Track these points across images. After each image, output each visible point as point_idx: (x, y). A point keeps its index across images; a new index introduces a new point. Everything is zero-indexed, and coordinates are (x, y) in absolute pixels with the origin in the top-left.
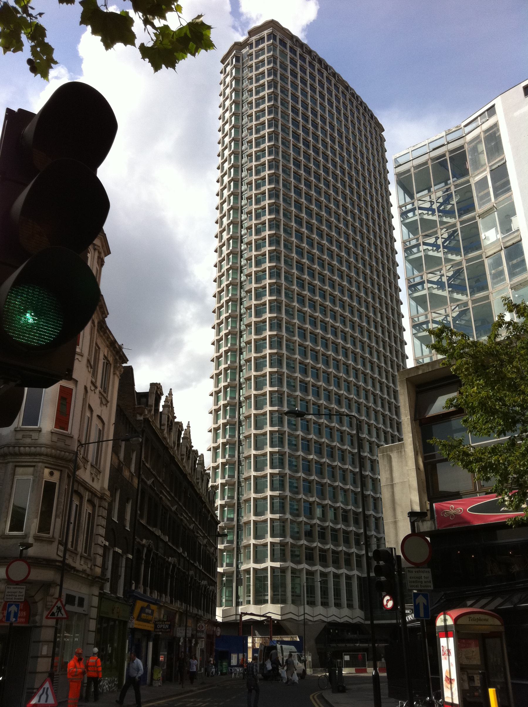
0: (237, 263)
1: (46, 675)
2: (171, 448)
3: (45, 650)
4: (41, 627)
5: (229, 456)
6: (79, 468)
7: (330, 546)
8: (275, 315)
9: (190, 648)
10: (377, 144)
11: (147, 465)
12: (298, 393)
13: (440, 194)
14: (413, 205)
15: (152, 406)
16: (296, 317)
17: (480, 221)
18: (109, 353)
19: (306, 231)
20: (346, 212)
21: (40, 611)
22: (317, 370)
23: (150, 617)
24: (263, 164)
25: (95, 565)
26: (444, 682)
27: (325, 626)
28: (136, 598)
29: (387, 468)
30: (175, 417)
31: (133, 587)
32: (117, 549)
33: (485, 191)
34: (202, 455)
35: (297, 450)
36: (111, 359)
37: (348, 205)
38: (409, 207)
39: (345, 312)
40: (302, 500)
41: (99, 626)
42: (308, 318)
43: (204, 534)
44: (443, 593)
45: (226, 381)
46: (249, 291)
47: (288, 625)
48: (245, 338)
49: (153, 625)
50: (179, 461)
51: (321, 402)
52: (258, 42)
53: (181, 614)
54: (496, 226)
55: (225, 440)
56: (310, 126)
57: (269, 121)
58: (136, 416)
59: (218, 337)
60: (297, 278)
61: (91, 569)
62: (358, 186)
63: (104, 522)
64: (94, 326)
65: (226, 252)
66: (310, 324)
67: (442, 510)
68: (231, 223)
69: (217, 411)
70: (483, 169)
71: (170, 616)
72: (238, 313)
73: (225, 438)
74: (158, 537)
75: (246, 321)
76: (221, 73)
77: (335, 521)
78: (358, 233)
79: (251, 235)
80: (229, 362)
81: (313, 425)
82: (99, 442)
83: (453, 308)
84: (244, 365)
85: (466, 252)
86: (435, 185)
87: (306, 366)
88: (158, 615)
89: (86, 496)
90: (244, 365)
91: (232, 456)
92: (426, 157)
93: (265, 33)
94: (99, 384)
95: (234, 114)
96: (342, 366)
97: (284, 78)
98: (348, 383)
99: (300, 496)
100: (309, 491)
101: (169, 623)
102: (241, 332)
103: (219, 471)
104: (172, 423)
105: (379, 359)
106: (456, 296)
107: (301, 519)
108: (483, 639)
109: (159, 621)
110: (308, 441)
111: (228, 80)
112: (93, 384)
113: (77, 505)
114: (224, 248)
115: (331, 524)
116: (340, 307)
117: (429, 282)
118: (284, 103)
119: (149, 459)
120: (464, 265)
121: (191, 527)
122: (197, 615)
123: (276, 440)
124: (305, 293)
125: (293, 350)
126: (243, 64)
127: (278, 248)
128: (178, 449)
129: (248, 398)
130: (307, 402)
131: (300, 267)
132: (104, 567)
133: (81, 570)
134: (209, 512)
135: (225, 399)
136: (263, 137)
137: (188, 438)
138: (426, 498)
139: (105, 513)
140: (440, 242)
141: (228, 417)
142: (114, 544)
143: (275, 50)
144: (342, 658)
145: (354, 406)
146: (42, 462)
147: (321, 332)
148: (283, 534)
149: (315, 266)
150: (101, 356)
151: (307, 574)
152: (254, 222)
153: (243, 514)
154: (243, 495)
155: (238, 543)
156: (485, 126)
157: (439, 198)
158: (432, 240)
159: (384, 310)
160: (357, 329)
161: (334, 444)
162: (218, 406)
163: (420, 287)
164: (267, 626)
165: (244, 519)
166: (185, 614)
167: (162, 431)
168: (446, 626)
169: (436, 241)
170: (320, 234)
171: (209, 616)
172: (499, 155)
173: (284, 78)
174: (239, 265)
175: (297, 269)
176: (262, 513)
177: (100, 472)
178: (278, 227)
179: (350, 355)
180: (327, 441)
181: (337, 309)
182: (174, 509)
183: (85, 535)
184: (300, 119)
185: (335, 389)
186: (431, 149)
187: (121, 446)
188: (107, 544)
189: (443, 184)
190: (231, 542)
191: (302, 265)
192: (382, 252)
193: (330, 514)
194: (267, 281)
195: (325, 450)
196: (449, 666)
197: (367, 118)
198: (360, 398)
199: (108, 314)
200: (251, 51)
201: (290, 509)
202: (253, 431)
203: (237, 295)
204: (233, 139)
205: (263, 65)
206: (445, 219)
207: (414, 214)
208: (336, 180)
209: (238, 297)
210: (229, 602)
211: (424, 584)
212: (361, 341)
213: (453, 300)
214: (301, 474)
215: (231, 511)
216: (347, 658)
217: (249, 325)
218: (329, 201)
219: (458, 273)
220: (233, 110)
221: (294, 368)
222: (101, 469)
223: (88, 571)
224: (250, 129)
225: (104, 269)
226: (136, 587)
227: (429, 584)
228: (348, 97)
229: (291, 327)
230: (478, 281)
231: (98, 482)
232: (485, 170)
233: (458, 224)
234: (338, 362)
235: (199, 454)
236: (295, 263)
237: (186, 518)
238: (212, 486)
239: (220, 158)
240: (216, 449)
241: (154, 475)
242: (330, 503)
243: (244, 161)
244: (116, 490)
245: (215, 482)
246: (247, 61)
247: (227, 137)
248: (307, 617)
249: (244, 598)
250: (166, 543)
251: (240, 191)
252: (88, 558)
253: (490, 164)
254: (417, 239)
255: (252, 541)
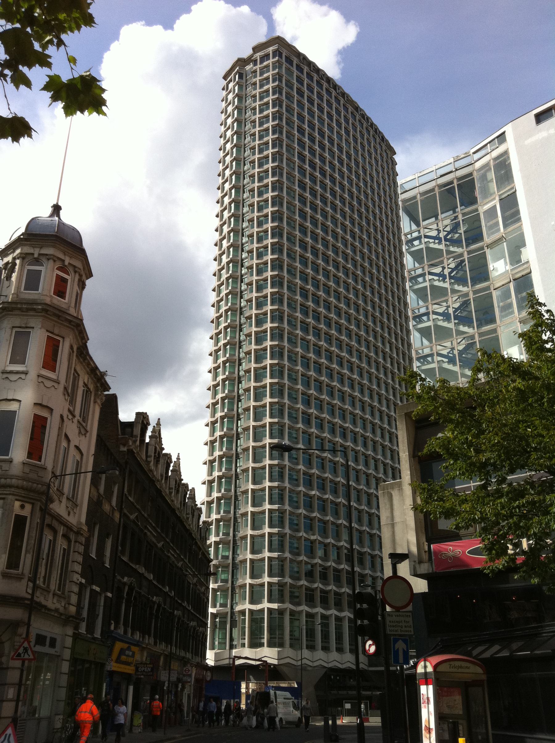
0: (237, 288)
1: (10, 720)
2: (158, 481)
3: (11, 693)
4: (7, 668)
5: (225, 490)
6: (52, 501)
7: (332, 587)
8: (276, 343)
9: (176, 692)
10: (388, 168)
11: (130, 498)
12: (300, 425)
13: (447, 222)
14: (419, 233)
15: (137, 436)
16: (299, 345)
17: (488, 252)
18: (90, 380)
19: (311, 257)
20: (354, 238)
21: (6, 651)
22: (321, 401)
23: (130, 660)
24: (266, 186)
25: (69, 604)
26: (423, 732)
27: (326, 673)
28: (115, 639)
29: (388, 506)
30: (163, 449)
31: (112, 627)
32: (94, 587)
33: (494, 221)
34: (193, 489)
35: (298, 485)
36: (91, 387)
37: (356, 230)
38: (415, 235)
39: (352, 341)
40: (303, 539)
41: (73, 669)
42: (312, 347)
43: (194, 572)
44: (439, 639)
45: (223, 411)
46: (250, 318)
47: (285, 669)
48: (244, 366)
49: (134, 668)
50: (166, 494)
51: (325, 435)
52: (263, 59)
53: (166, 656)
54: (505, 257)
55: (221, 474)
56: (317, 147)
57: (273, 141)
58: (119, 447)
59: (216, 365)
60: (301, 305)
61: (65, 608)
62: (368, 211)
63: (80, 559)
64: (73, 352)
65: (226, 276)
66: (314, 353)
67: (440, 551)
68: (232, 245)
69: (212, 442)
70: (492, 197)
71: (154, 659)
72: (237, 340)
73: (221, 471)
74: (142, 575)
75: (245, 348)
76: (223, 89)
77: (338, 561)
78: (367, 260)
79: (252, 259)
80: (226, 392)
81: (315, 459)
82: (77, 473)
83: (459, 340)
84: (243, 395)
85: (474, 283)
86: (442, 213)
87: (309, 396)
88: (139, 656)
89: (61, 530)
90: (243, 395)
91: (228, 490)
92: (433, 184)
93: (271, 49)
94: (77, 412)
95: (236, 132)
96: (348, 397)
97: (289, 97)
98: (354, 416)
99: (301, 534)
100: (310, 528)
101: (151, 666)
102: (240, 360)
103: (214, 505)
104: (159, 454)
105: (387, 391)
106: (462, 328)
107: (301, 558)
108: (466, 687)
109: (141, 664)
110: (310, 476)
111: (230, 97)
112: (71, 413)
113: (50, 540)
114: (224, 272)
115: (333, 564)
116: (346, 337)
117: (434, 313)
118: (289, 123)
119: (133, 492)
120: (471, 296)
121: (180, 564)
122: (184, 658)
123: (276, 474)
124: (309, 320)
125: (295, 380)
126: (246, 81)
127: (281, 274)
128: (166, 482)
129: (247, 429)
130: (309, 435)
131: (305, 294)
132: (79, 606)
133: (53, 608)
134: (200, 549)
135: (222, 430)
136: (267, 157)
137: (177, 471)
138: (424, 539)
139: (81, 549)
140: (446, 272)
141: (224, 449)
142: (91, 582)
143: (280, 67)
144: (342, 706)
145: (360, 440)
146: (13, 495)
147: (325, 362)
148: (281, 574)
149: (320, 293)
150: (81, 384)
151: (306, 617)
152: (255, 245)
153: (239, 552)
154: (239, 532)
155: (232, 582)
156: (495, 154)
157: (446, 226)
158: (438, 270)
159: (394, 340)
160: (364, 359)
161: (338, 479)
162: (214, 438)
163: (425, 318)
164: (263, 671)
165: (240, 557)
166: (169, 657)
167: (148, 463)
168: (426, 673)
169: (443, 271)
170: (326, 259)
171: (198, 659)
172: (509, 184)
173: (289, 97)
174: (239, 290)
175: (301, 296)
176: (260, 552)
177: (77, 506)
178: (281, 251)
179: (357, 387)
180: (330, 476)
181: (343, 338)
182: (160, 545)
183: (59, 572)
184: (306, 140)
185: (339, 422)
186: (438, 175)
187: (101, 479)
188: (83, 581)
189: (451, 212)
190: (225, 581)
191: (307, 291)
192: (392, 280)
193: (333, 555)
194: (269, 308)
195: (328, 485)
196: (428, 714)
197: (378, 140)
198: (366, 432)
199: (88, 339)
200: (255, 68)
201: (290, 547)
202: (251, 465)
203: (236, 321)
204: (235, 159)
205: (268, 83)
206: (452, 249)
207: (420, 242)
208: (344, 204)
209: (238, 323)
210: (222, 645)
211: (404, 629)
212: (368, 372)
213: (459, 333)
214: (302, 511)
215: (226, 548)
216: (348, 706)
217: (249, 353)
218: (336, 226)
219: (465, 304)
220: (235, 129)
221: (296, 399)
222: (79, 502)
223: (62, 610)
224: (253, 148)
225: (85, 292)
226: (116, 628)
227: (409, 629)
228: (357, 118)
229: (293, 355)
230: (486, 313)
231: (74, 516)
232: (494, 199)
233: (466, 253)
234: (343, 393)
235: (190, 488)
236: (299, 289)
237: (173, 555)
238: (204, 522)
239: (221, 177)
240: (211, 482)
241: (138, 509)
242: (333, 541)
243: (246, 181)
244: (95, 524)
245: (209, 517)
246: (251, 78)
247: (229, 156)
248: (304, 661)
249: (239, 641)
250: (150, 581)
251: (241, 213)
252: (62, 595)
253: (501, 149)
254: (423, 268)
255: (248, 581)
